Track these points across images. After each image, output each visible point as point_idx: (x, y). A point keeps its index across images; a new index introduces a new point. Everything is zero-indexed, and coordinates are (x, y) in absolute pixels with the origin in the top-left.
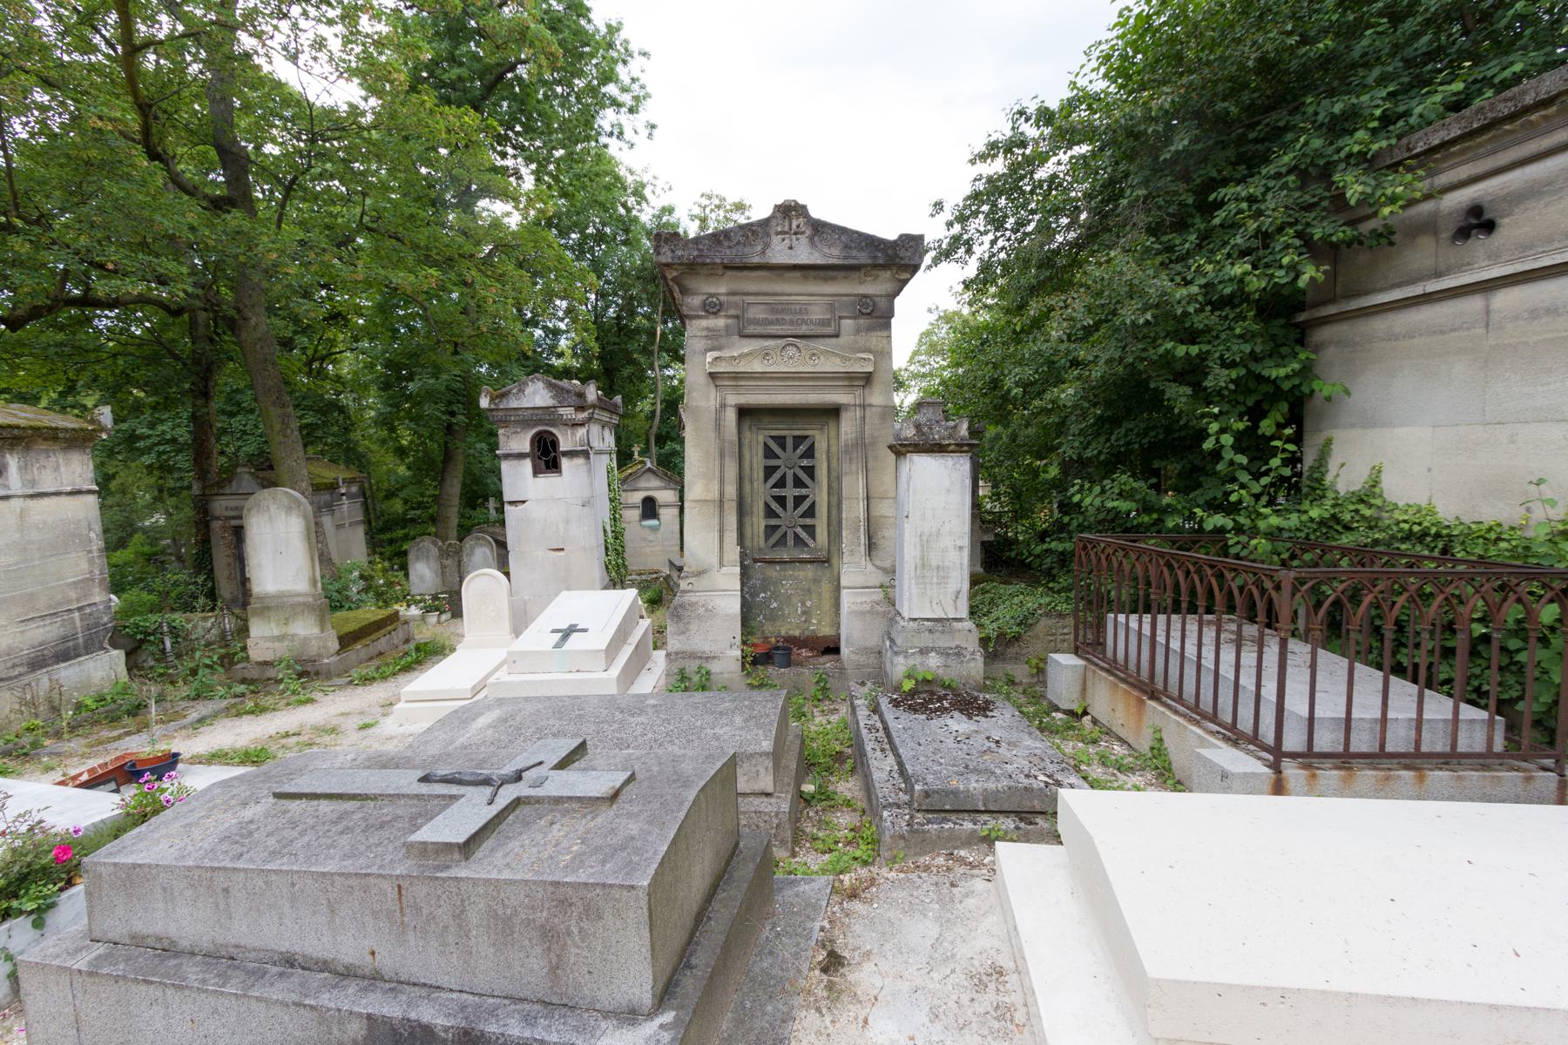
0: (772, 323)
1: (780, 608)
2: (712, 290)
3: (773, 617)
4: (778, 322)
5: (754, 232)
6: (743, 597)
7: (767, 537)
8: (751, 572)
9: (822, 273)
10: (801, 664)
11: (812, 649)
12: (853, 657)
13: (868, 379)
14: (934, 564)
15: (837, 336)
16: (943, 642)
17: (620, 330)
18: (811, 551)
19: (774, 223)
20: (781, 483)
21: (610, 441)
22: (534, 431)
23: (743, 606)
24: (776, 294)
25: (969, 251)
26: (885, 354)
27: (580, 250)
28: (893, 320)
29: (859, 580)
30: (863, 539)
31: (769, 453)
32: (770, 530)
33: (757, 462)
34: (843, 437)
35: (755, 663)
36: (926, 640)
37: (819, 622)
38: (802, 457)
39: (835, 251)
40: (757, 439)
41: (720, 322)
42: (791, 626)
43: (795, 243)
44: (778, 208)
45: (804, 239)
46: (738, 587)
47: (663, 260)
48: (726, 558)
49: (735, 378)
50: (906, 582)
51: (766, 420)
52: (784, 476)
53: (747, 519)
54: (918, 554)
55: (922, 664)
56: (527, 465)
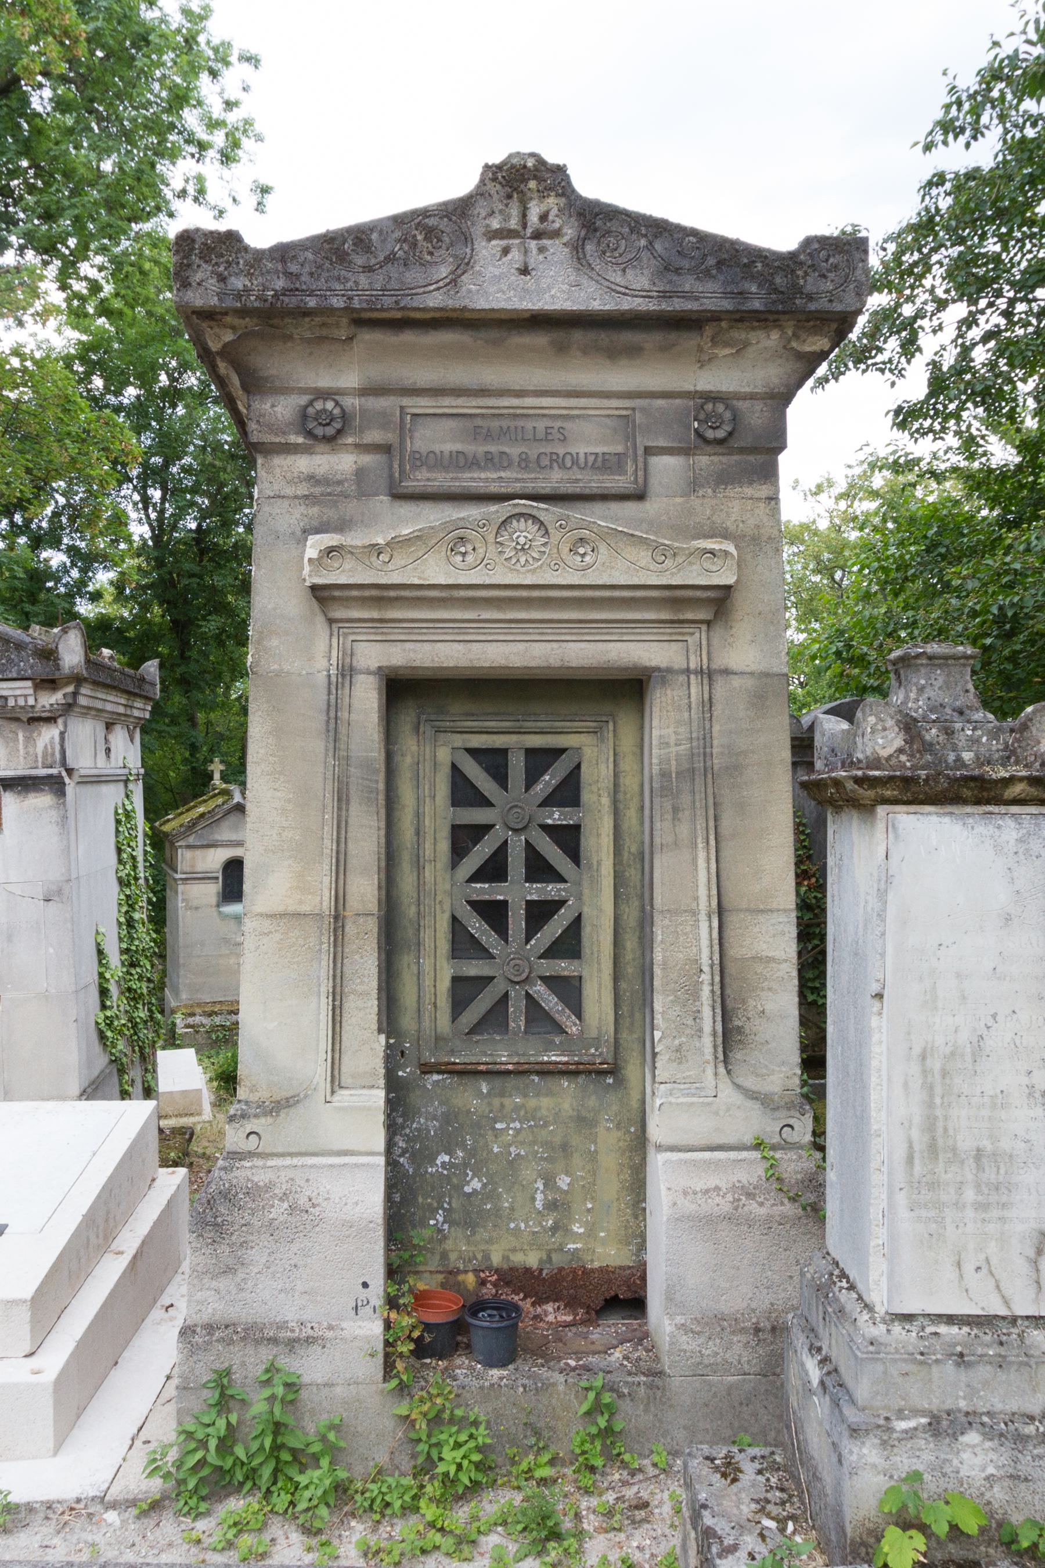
0: (473, 463)
1: (489, 1194)
2: (324, 381)
3: (470, 1217)
4: (490, 461)
5: (430, 233)
6: (392, 1164)
7: (458, 1005)
8: (414, 1098)
9: (604, 337)
10: (541, 1352)
11: (571, 1304)
12: (687, 1343)
13: (719, 602)
14: (966, 1143)
15: (640, 497)
16: (1004, 1395)
17: (202, 552)
18: (569, 1044)
19: (481, 209)
20: (494, 869)
21: (127, 752)
23: (391, 1187)
24: (483, 392)
25: (910, 347)
27: (139, 415)
28: (782, 458)
30: (708, 1019)
31: (463, 792)
32: (463, 991)
33: (432, 812)
34: (655, 755)
35: (421, 1350)
36: (949, 1389)
37: (591, 1232)
38: (548, 802)
39: (640, 279)
40: (434, 756)
41: (343, 462)
42: (517, 1242)
43: (534, 259)
45: (557, 249)
46: (379, 1142)
47: (197, 299)
48: (349, 1065)
49: (380, 602)
50: (877, 1201)
51: (457, 707)
52: (502, 849)
53: (406, 962)
55: (939, 1468)
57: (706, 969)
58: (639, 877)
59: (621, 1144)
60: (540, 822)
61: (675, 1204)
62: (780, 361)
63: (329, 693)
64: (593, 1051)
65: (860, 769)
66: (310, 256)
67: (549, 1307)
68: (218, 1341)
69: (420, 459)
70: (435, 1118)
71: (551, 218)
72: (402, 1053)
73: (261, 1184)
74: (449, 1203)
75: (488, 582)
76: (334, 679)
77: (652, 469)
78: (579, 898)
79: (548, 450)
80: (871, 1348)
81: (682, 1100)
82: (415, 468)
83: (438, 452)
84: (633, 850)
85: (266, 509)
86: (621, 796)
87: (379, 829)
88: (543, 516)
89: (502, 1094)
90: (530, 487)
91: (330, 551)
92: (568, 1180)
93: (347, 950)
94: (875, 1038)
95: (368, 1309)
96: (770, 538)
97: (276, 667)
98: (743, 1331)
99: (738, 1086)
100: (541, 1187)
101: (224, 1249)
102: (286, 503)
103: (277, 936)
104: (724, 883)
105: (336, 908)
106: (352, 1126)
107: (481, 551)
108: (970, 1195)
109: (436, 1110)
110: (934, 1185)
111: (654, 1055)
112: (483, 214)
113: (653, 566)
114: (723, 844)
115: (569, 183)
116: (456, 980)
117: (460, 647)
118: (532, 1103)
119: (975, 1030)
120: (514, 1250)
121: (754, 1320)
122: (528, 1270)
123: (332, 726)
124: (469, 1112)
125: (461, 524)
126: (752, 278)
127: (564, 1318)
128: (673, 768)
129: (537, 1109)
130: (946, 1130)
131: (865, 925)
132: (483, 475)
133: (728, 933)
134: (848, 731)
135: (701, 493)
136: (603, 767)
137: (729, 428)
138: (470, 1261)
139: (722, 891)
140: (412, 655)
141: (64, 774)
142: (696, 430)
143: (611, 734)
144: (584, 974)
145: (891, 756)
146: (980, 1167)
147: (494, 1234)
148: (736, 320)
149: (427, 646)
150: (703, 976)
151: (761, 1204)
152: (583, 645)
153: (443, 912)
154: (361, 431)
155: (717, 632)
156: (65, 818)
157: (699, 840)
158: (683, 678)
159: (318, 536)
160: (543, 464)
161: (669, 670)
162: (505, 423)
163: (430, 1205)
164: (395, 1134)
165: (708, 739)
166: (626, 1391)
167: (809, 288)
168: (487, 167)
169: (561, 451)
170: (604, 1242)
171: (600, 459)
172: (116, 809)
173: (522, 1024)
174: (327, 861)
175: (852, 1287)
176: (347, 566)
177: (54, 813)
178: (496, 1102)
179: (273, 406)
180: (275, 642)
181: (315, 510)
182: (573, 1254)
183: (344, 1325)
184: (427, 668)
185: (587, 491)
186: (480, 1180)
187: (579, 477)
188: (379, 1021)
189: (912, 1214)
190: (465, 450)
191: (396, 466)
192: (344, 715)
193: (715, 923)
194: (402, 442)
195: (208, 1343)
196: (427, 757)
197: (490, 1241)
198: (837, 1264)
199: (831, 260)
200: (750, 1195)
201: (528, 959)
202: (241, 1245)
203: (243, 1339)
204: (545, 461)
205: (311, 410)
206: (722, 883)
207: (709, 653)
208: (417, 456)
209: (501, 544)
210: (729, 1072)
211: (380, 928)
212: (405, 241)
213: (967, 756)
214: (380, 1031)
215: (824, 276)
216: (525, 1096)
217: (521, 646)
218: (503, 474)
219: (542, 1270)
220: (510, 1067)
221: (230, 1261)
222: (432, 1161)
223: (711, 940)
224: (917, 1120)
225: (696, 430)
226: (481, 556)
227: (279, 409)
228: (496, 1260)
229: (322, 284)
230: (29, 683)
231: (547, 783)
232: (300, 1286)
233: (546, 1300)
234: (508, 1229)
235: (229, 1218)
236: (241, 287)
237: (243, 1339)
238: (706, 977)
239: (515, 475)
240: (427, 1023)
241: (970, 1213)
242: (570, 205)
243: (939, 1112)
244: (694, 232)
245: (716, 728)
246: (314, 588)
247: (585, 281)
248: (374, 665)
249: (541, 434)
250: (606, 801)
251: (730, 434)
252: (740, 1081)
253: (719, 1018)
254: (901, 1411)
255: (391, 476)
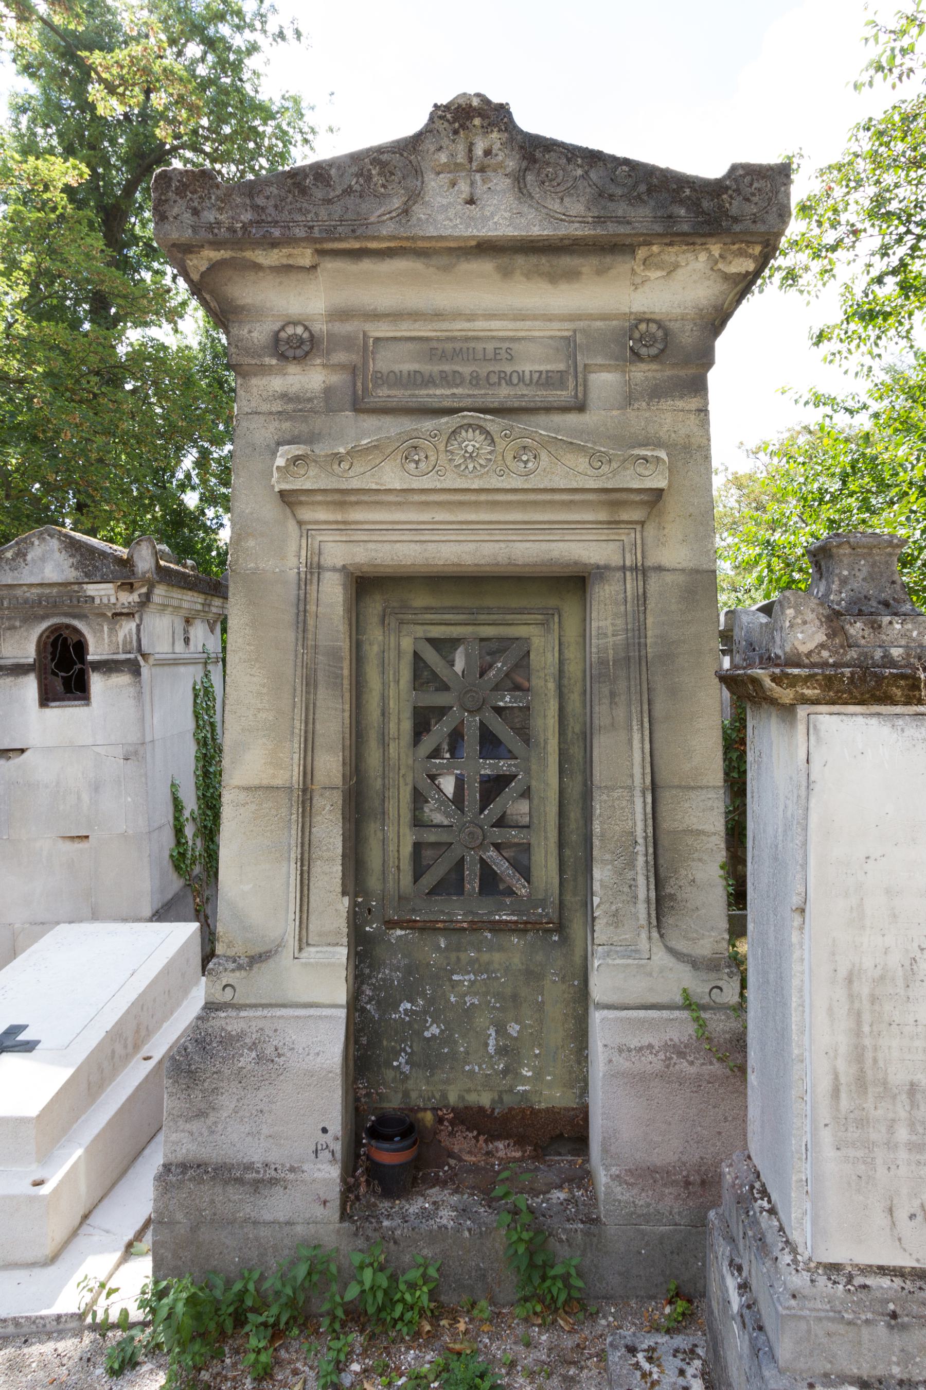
0: (429, 381)
1: (446, 1039)
3: (430, 1059)
4: (446, 379)
5: (383, 165)
11: (520, 1141)
14: (898, 1076)
15: (581, 408)
19: (429, 145)
22: (45, 625)
26: (693, 452)
29: (637, 988)
33: (392, 694)
37: (538, 1075)
39: (576, 207)
40: (394, 647)
42: (472, 1084)
43: (480, 188)
44: (440, 113)
45: (501, 183)
46: (341, 996)
53: (372, 828)
54: (843, 1043)
56: (30, 686)
57: (640, 841)
58: (582, 754)
59: (566, 996)
60: (493, 703)
61: (610, 1061)
62: (707, 283)
63: (299, 588)
64: (540, 910)
65: (777, 665)
66: (274, 190)
67: (500, 1145)
68: (190, 1180)
69: (381, 378)
70: (398, 969)
71: (494, 152)
72: (370, 911)
73: (234, 1033)
74: (411, 1047)
75: (439, 486)
76: (303, 576)
77: (590, 383)
78: (528, 772)
79: (497, 368)
80: (793, 1302)
81: (618, 961)
82: (376, 386)
83: (397, 370)
84: (577, 729)
85: (244, 424)
86: (565, 682)
87: (343, 711)
88: (489, 427)
89: (458, 949)
90: (479, 402)
91: (295, 460)
92: (517, 1027)
93: (314, 820)
94: (796, 955)
95: (326, 1155)
96: (699, 447)
97: (252, 565)
98: (674, 1183)
99: (671, 951)
100: (494, 1034)
101: (197, 1095)
102: (262, 418)
103: (253, 807)
104: (658, 761)
105: (304, 782)
106: (319, 981)
107: (432, 459)
108: (903, 1134)
109: (399, 962)
110: (862, 1123)
111: (594, 919)
112: (432, 149)
113: (590, 472)
114: (656, 727)
115: (511, 120)
116: (418, 847)
117: (417, 547)
118: (485, 957)
119: (907, 951)
120: (469, 1091)
121: (684, 1173)
122: (481, 1109)
123: (301, 618)
124: (428, 964)
125: (414, 434)
126: (681, 202)
127: (514, 1154)
128: (611, 657)
129: (489, 963)
130: (875, 1061)
131: (785, 831)
132: (438, 392)
133: (663, 809)
134: (767, 624)
135: (636, 406)
136: (549, 655)
137: (661, 347)
138: (429, 1100)
139: (656, 769)
140: (373, 554)
141: (140, 658)
142: (631, 348)
143: (556, 626)
144: (533, 841)
145: (811, 652)
146: (914, 1104)
147: (451, 1076)
148: (666, 244)
149: (387, 547)
150: (638, 848)
151: (692, 1063)
152: (528, 545)
153: (406, 784)
154: (328, 354)
155: (651, 530)
156: (140, 693)
157: (634, 723)
158: (619, 574)
159: (287, 447)
160: (491, 381)
161: (607, 567)
162: (458, 345)
163: (393, 1048)
164: (362, 983)
165: (642, 630)
166: (564, 1237)
167: (734, 211)
168: (436, 106)
169: (508, 370)
170: (550, 1085)
171: (544, 376)
172: (195, 684)
173: (477, 885)
174: (296, 739)
175: (772, 1211)
176: (311, 473)
177: (132, 689)
178: (453, 956)
179: (250, 332)
180: (251, 543)
181: (287, 425)
182: (522, 1095)
183: (305, 1168)
184: (388, 566)
185: (532, 405)
186: (438, 1027)
187: (525, 392)
188: (343, 884)
189: (839, 1153)
190: (422, 370)
191: (359, 384)
192: (312, 608)
193: (649, 800)
194: (365, 363)
195: (182, 1182)
196: (392, 645)
197: (447, 1082)
198: (758, 1176)
199: (755, 185)
200: (681, 1054)
201: (481, 828)
202: (213, 1091)
203: (213, 1178)
204: (494, 379)
205: (283, 335)
206: (655, 762)
207: (643, 552)
208: (379, 375)
209: (452, 453)
210: (662, 936)
211: (344, 801)
212: (362, 175)
213: (896, 652)
214: (344, 893)
215: (748, 200)
216: (479, 950)
217: (472, 546)
218: (455, 391)
219: (493, 1109)
220: (465, 925)
221: (203, 1106)
222: (396, 1009)
223: (645, 814)
224: (843, 1049)
225: (631, 348)
226: (433, 463)
227: (255, 334)
228: (452, 1098)
229: (285, 216)
230: (111, 585)
231: (500, 669)
232: (265, 1130)
233: (499, 1138)
234: (464, 1071)
235: (202, 1066)
236: (213, 220)
237: (213, 1178)
238: (640, 849)
239: (467, 392)
240: (391, 884)
241: (903, 1154)
242: (511, 139)
243: (867, 1042)
244: (626, 162)
245: (650, 621)
246: (282, 493)
247: (525, 209)
248: (339, 563)
249: (490, 355)
250: (551, 685)
251: (662, 351)
252: (673, 944)
253: (652, 887)
254: (826, 1375)
255: (355, 392)
